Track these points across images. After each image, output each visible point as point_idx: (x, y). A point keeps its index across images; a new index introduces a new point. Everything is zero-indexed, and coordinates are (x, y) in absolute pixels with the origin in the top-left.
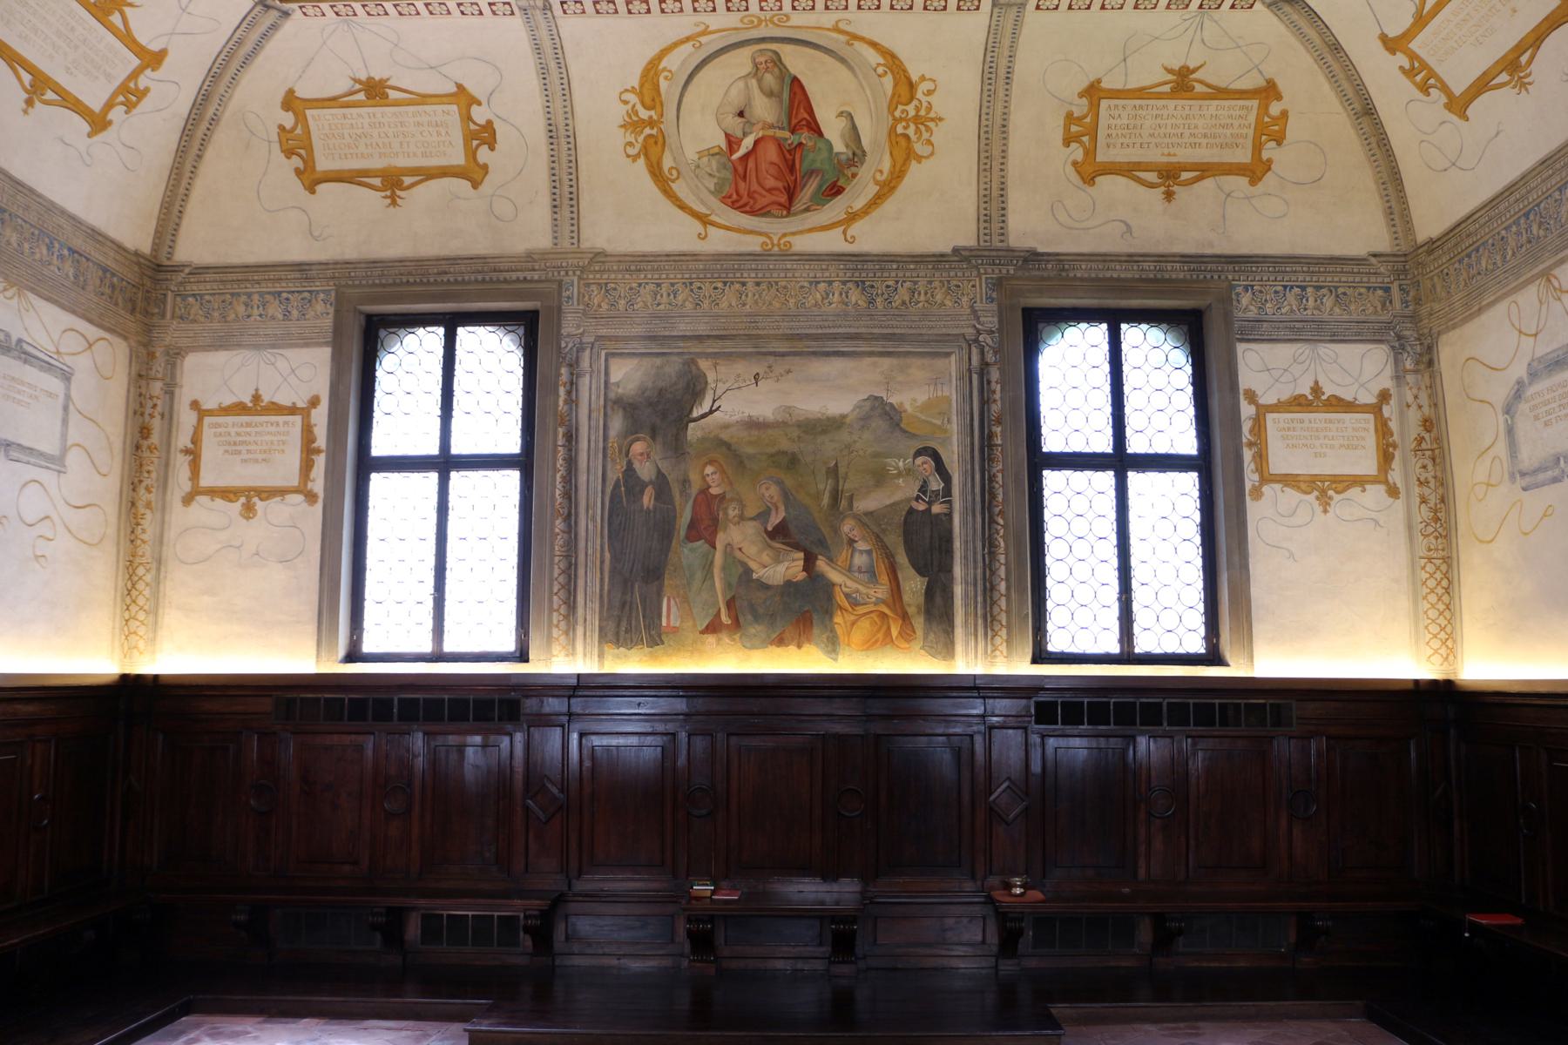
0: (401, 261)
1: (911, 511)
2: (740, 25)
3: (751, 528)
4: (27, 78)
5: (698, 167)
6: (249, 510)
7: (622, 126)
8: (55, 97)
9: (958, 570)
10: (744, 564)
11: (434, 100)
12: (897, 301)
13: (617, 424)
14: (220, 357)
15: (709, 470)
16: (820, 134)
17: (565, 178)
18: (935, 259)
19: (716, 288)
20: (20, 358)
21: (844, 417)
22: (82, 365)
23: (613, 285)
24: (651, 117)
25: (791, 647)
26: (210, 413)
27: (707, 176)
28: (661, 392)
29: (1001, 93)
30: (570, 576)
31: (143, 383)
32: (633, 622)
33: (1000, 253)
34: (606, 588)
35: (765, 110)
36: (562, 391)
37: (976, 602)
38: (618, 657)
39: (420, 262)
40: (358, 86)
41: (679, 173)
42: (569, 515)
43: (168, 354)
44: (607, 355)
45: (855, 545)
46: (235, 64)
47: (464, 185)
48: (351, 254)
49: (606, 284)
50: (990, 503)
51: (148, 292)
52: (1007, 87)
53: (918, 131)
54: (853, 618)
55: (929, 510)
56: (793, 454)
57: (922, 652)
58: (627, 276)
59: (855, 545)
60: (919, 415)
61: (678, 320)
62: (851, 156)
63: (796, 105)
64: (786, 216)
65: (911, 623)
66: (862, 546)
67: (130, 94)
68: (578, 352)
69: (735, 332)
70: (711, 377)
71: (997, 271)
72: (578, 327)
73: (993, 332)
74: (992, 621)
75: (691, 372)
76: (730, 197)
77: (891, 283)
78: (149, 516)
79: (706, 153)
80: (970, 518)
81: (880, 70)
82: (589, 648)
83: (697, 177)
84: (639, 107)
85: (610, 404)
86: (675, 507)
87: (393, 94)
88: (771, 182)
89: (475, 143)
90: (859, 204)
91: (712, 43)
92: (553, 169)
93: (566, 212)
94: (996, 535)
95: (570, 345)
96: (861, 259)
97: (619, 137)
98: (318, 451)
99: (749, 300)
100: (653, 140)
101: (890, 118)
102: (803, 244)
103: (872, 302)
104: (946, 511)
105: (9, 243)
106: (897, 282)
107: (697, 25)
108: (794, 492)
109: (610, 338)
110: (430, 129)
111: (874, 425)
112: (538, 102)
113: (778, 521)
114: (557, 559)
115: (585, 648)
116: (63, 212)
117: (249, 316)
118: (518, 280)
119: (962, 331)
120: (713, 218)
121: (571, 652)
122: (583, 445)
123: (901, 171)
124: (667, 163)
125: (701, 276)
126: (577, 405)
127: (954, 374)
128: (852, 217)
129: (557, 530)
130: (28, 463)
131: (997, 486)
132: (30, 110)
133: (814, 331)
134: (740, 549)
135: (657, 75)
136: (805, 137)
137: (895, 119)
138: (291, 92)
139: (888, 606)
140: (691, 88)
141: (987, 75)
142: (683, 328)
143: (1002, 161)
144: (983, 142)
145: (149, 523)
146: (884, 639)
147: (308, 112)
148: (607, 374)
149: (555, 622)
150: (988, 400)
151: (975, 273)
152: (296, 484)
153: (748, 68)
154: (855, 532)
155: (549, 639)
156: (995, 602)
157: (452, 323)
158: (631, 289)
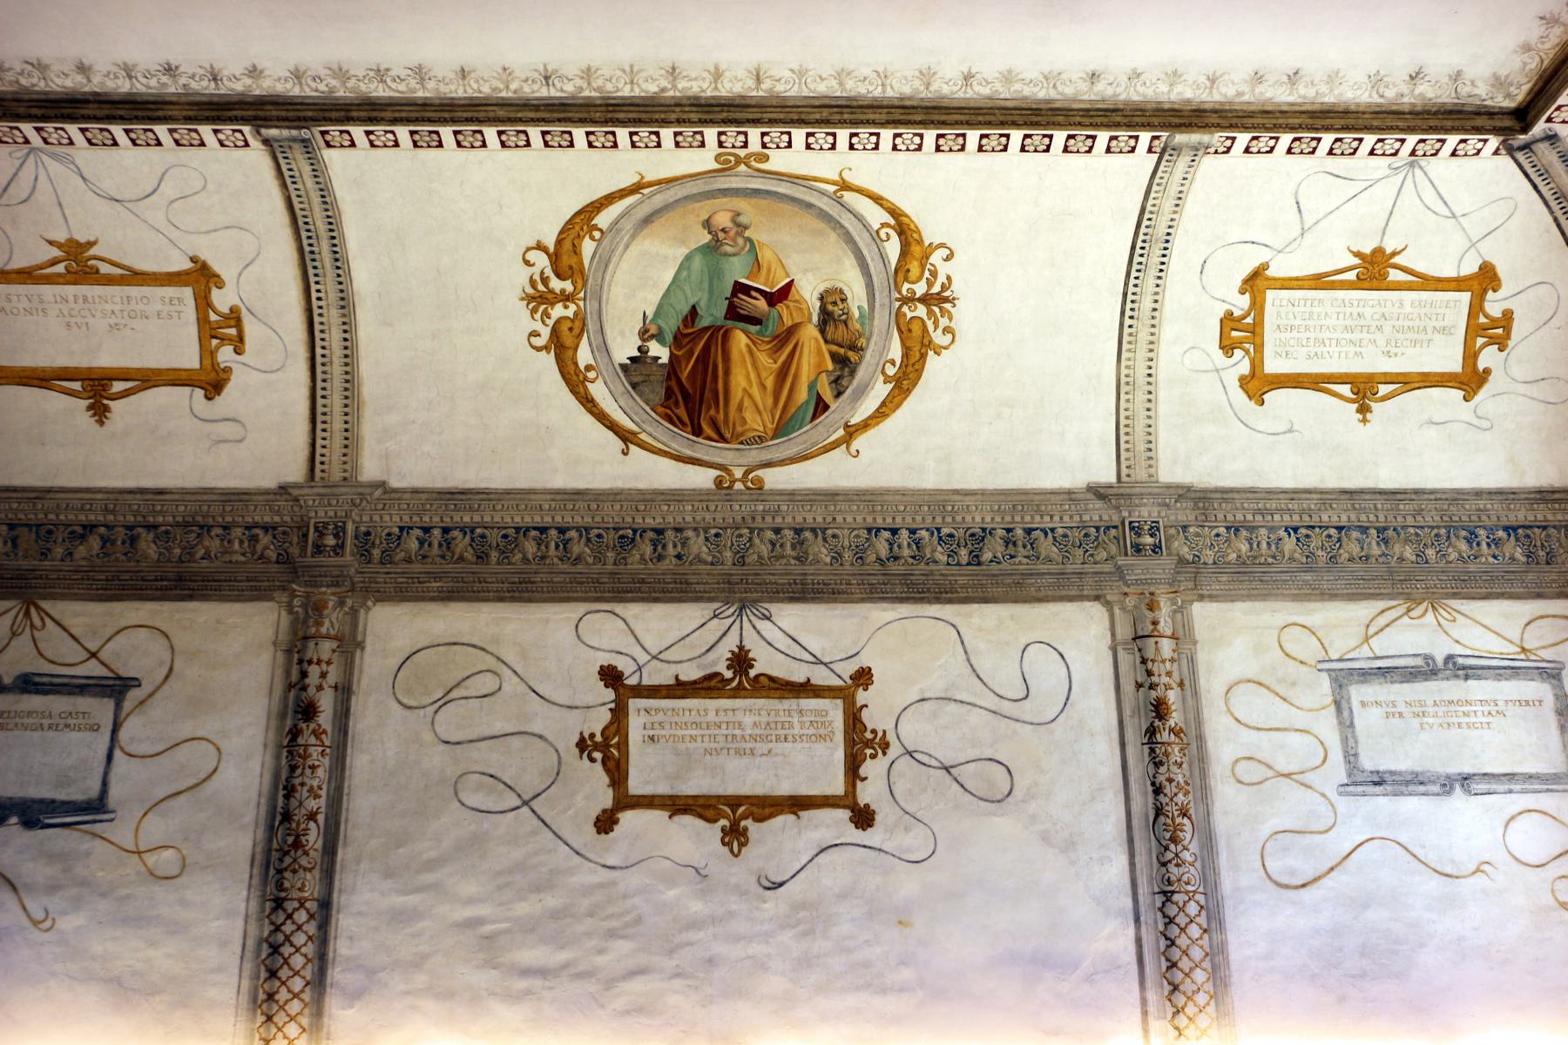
4: (1345, 390)
8: (1392, 387)
20: (1457, 676)
105: (1401, 559)
116: (1478, 493)
130: (1511, 791)
132: (1368, 416)
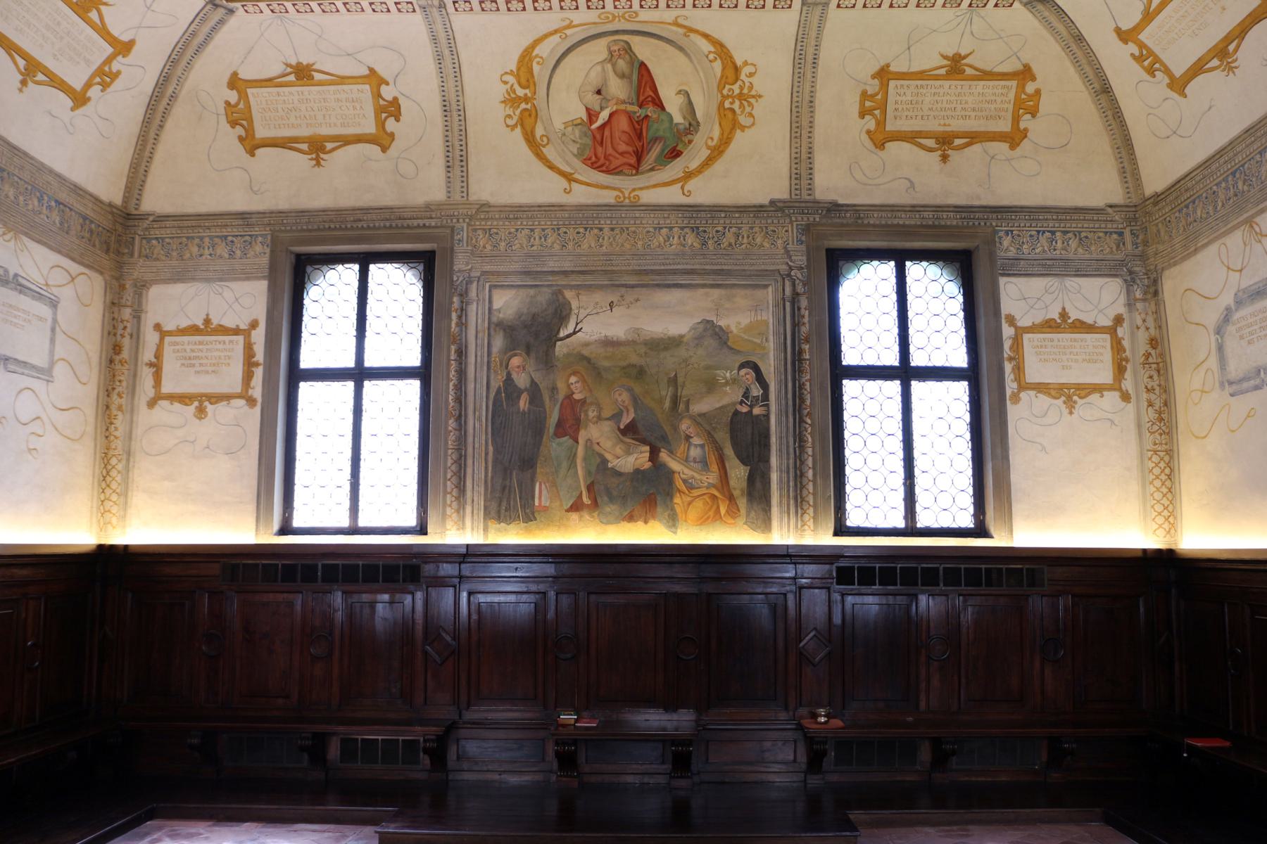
0: (324, 211)
1: (736, 413)
2: (598, 20)
3: (607, 427)
4: (21, 63)
5: (564, 135)
6: (201, 412)
7: (502, 102)
8: (44, 78)
9: (774, 461)
10: (601, 456)
11: (350, 81)
12: (725, 243)
13: (499, 342)
14: (177, 289)
15: (573, 379)
16: (663, 108)
17: (457, 144)
18: (755, 209)
19: (578, 233)
20: (16, 289)
21: (682, 336)
22: (66, 295)
23: (495, 231)
24: (526, 95)
25: (639, 523)
26: (170, 333)
27: (571, 143)
28: (534, 316)
29: (809, 75)
30: (460, 465)
31: (116, 309)
32: (512, 503)
33: (808, 205)
34: (490, 475)
35: (618, 89)
36: (454, 316)
37: (789, 486)
38: (499, 530)
39: (339, 211)
40: (289, 70)
41: (548, 140)
42: (460, 416)
43: (136, 286)
44: (490, 286)
45: (691, 440)
46: (190, 52)
47: (375, 150)
48: (283, 205)
49: (490, 229)
50: (800, 406)
51: (119, 235)
52: (813, 70)
53: (741, 106)
54: (689, 499)
55: (750, 412)
56: (641, 367)
57: (745, 526)
58: (507, 223)
59: (691, 440)
60: (743, 335)
61: (548, 258)
62: (688, 126)
63: (643, 85)
64: (635, 175)
65: (736, 503)
66: (696, 441)
67: (105, 76)
68: (467, 284)
69: (594, 268)
70: (574, 304)
71: (805, 219)
72: (467, 264)
73: (802, 268)
74: (801, 502)
75: (558, 300)
76: (590, 159)
77: (720, 229)
78: (120, 416)
79: (571, 123)
80: (784, 419)
81: (711, 57)
82: (476, 524)
83: (563, 143)
84: (516, 87)
85: (493, 326)
86: (545, 410)
87: (317, 76)
88: (623, 147)
89: (384, 115)
90: (694, 165)
91: (575, 35)
92: (447, 136)
93: (457, 171)
94: (805, 432)
95: (461, 279)
96: (695, 209)
97: (500, 111)
98: (257, 364)
99: (606, 243)
100: (527, 113)
101: (719, 95)
102: (649, 197)
103: (704, 244)
104: (764, 413)
105: (7, 196)
106: (725, 228)
107: (563, 20)
108: (641, 398)
109: (493, 273)
110: (348, 104)
111: (706, 343)
112: (435, 83)
113: (628, 421)
114: (450, 452)
115: (473, 523)
116: (51, 171)
117: (201, 255)
118: (418, 226)
119: (778, 267)
120: (576, 176)
121: (462, 527)
122: (471, 359)
123: (728, 138)
124: (539, 131)
125: (567, 223)
126: (466, 327)
127: (771, 302)
128: (689, 175)
129: (450, 428)
130: (23, 374)
131: (806, 392)
132: (24, 89)
133: (657, 268)
134: (598, 444)
135: (531, 60)
136: (650, 110)
137: (723, 96)
138: (235, 74)
139: (718, 489)
140: (558, 71)
141: (797, 61)
142: (552, 265)
143: (810, 130)
144: (795, 114)
145: (120, 422)
146: (714, 516)
147: (249, 91)
148: (490, 302)
149: (448, 502)
150: (799, 323)
151: (788, 221)
152: (240, 391)
153: (604, 55)
154: (691, 430)
155: (444, 516)
156: (804, 487)
157: (365, 261)
158: (510, 233)
